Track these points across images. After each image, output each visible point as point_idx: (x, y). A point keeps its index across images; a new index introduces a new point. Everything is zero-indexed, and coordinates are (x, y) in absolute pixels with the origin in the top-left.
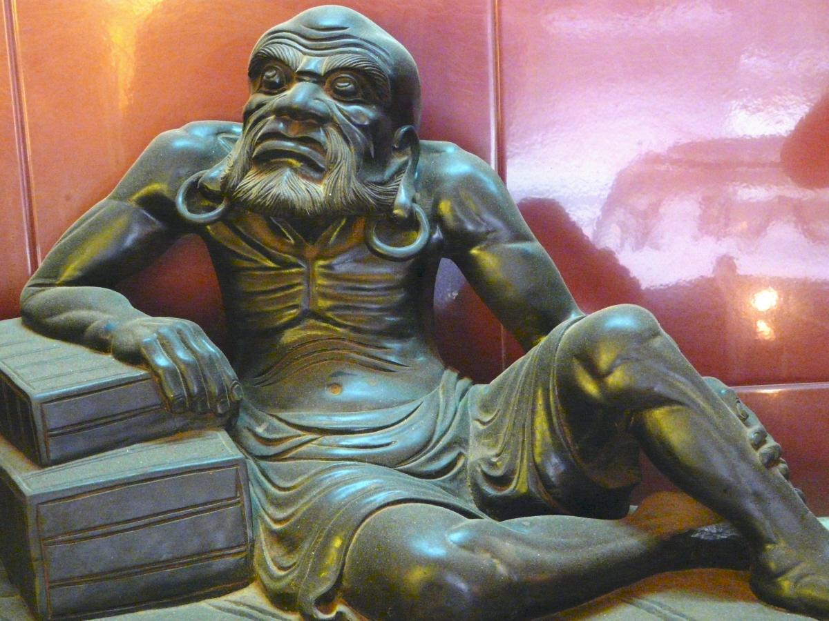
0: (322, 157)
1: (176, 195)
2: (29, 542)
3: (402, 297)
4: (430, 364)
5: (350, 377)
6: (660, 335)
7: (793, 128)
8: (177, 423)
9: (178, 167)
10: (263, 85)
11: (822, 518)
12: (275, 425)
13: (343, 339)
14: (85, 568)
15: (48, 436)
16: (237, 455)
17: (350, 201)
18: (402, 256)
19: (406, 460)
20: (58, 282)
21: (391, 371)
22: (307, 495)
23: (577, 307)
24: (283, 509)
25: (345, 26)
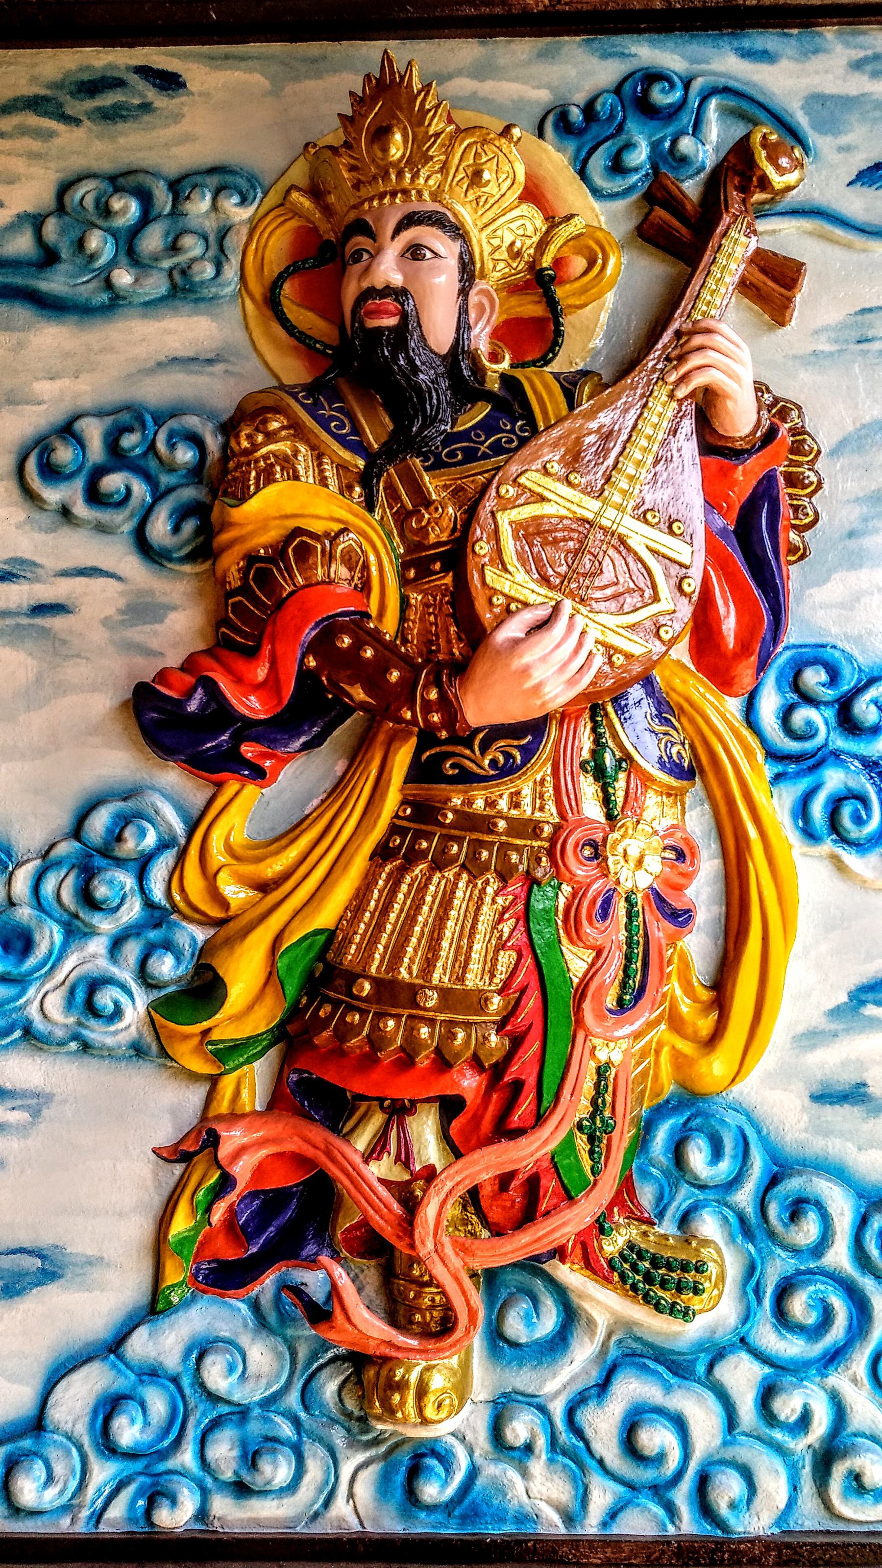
0: (513, 518)
1: (111, 88)
2: (34, 139)
3: (521, 656)
4: (208, 333)
5: (261, 839)
6: (699, 1042)
7: (873, 1179)
8: (761, 489)
9: (674, 612)
10: (515, 139)
11: (280, 1050)
12: (807, 118)
13: (815, 1274)
14: (733, 1506)
15: (707, 1377)
16: (851, 603)
17: (120, 618)
18: (150, 865)
19: (869, 233)
20: (581, 1444)
21: (65, 574)
22: (426, 1147)
23: (152, 998)
24: (714, 884)
25: (230, 826)
